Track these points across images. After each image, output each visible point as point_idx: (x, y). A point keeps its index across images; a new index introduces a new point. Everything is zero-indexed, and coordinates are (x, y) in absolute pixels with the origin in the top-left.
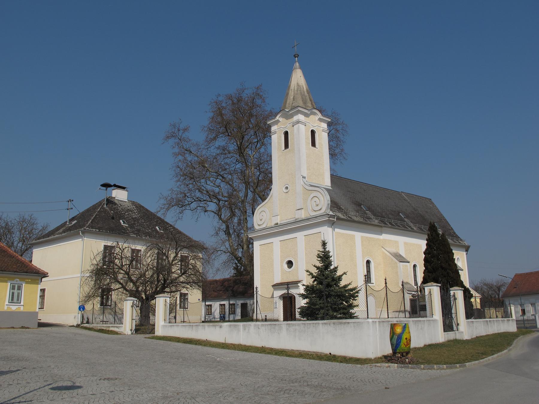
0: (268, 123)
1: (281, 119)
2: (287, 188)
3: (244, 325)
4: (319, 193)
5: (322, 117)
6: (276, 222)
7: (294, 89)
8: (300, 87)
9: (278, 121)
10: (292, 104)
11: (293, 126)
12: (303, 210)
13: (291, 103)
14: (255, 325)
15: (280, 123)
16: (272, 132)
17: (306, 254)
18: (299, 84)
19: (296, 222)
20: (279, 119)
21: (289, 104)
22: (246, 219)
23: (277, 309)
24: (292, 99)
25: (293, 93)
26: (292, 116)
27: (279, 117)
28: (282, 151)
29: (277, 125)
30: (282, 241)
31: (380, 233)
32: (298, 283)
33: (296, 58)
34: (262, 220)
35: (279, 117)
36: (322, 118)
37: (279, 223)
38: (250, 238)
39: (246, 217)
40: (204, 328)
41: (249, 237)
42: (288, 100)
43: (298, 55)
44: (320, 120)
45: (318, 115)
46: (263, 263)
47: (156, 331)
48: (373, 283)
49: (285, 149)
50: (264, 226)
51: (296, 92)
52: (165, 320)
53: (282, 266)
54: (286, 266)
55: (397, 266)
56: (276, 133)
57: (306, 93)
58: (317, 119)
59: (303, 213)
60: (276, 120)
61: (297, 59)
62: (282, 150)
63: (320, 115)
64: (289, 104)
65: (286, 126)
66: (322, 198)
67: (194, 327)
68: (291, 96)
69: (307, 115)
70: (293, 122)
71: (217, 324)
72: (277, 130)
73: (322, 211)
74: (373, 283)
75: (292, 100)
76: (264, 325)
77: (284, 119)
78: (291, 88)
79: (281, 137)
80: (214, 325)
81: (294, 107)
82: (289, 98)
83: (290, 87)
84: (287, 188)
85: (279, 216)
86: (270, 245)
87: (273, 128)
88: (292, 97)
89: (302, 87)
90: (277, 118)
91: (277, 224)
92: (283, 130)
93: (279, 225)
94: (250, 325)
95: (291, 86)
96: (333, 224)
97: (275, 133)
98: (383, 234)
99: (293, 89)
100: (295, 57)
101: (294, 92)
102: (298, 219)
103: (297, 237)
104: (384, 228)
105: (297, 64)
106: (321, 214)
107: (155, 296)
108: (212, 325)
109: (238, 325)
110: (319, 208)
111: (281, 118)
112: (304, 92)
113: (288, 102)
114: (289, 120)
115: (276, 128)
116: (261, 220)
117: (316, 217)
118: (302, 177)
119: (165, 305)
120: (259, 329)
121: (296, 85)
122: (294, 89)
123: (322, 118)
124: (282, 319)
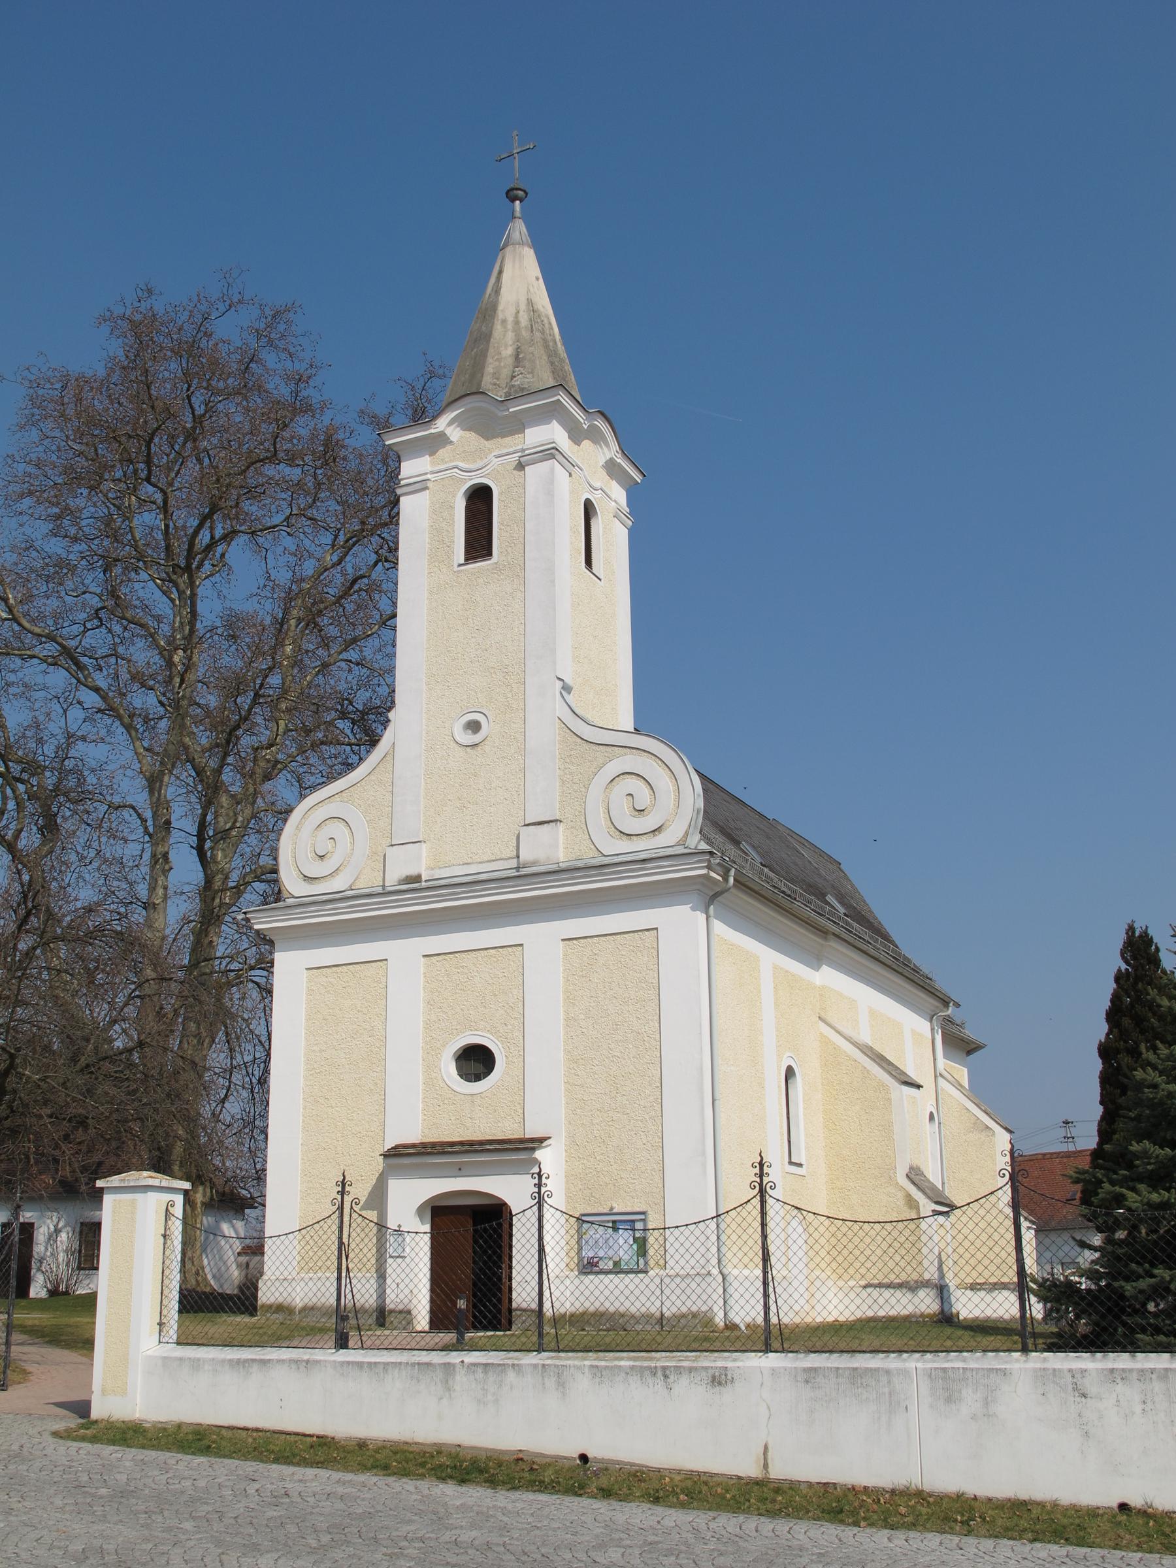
0: (387, 443)
1: (455, 433)
2: (474, 726)
3: (944, 1370)
4: (651, 761)
5: (620, 460)
6: (413, 871)
7: (517, 322)
8: (539, 316)
9: (441, 440)
10: (513, 377)
11: (520, 467)
12: (561, 827)
13: (505, 373)
14: (1042, 1376)
15: (448, 447)
16: (403, 483)
17: (570, 1022)
18: (535, 307)
19: (522, 875)
20: (448, 431)
21: (496, 375)
22: (165, 856)
23: (403, 1265)
24: (510, 361)
25: (510, 336)
26: (518, 425)
27: (450, 424)
28: (456, 569)
29: (432, 454)
30: (440, 958)
31: (815, 960)
32: (534, 1149)
33: (518, 202)
34: (325, 859)
35: (450, 424)
36: (619, 461)
37: (424, 878)
38: (258, 931)
39: (166, 849)
40: (561, 1385)
41: (256, 927)
42: (489, 360)
43: (525, 191)
44: (611, 468)
45: (608, 446)
46: (321, 1051)
47: (104, 1392)
48: (800, 1165)
49: (466, 560)
50: (338, 884)
51: (525, 334)
52: (161, 1324)
53: (431, 1067)
54: (450, 1068)
55: (889, 1099)
56: (426, 488)
57: (560, 348)
58: (602, 461)
59: (424, 854)
60: (433, 431)
61: (522, 208)
62: (456, 565)
63: (611, 451)
64: (496, 375)
65: (476, 466)
66: (663, 781)
67: (461, 1379)
68: (506, 348)
69: (576, 435)
70: (523, 450)
71: (686, 1364)
72: (429, 476)
73: (668, 839)
74: (800, 1165)
75: (510, 361)
76: (1135, 1375)
77: (471, 435)
78: (500, 315)
79: (452, 508)
80: (653, 1371)
81: (522, 389)
82: (491, 351)
83: (493, 307)
84: (474, 726)
85: (423, 845)
86: (372, 969)
87: (410, 469)
88: (508, 352)
89: (546, 321)
90: (442, 424)
91: (417, 879)
92: (464, 481)
93: (424, 884)
94: (1004, 1373)
95: (500, 308)
96: (714, 897)
97: (421, 486)
98: (825, 969)
99: (510, 319)
100: (513, 200)
101: (514, 331)
102: (534, 863)
103: (521, 945)
104: (834, 944)
105: (518, 229)
106: (663, 853)
107: (100, 1184)
108: (632, 1367)
109: (888, 1372)
110: (649, 823)
111: (459, 429)
112: (555, 341)
113: (490, 369)
114: (499, 440)
115: (429, 469)
116: (322, 857)
117: (644, 861)
118: (559, 684)
119: (164, 1236)
120: (1084, 1396)
121: (523, 307)
122: (517, 322)
123: (619, 465)
124: (422, 1318)
